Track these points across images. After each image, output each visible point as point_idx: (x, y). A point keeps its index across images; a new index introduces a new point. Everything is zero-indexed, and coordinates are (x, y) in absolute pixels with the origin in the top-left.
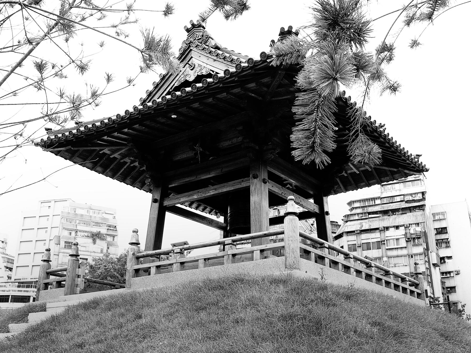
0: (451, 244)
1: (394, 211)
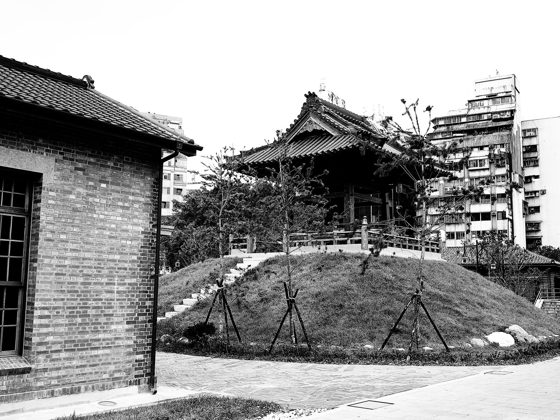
0: (540, 163)
1: (480, 131)
